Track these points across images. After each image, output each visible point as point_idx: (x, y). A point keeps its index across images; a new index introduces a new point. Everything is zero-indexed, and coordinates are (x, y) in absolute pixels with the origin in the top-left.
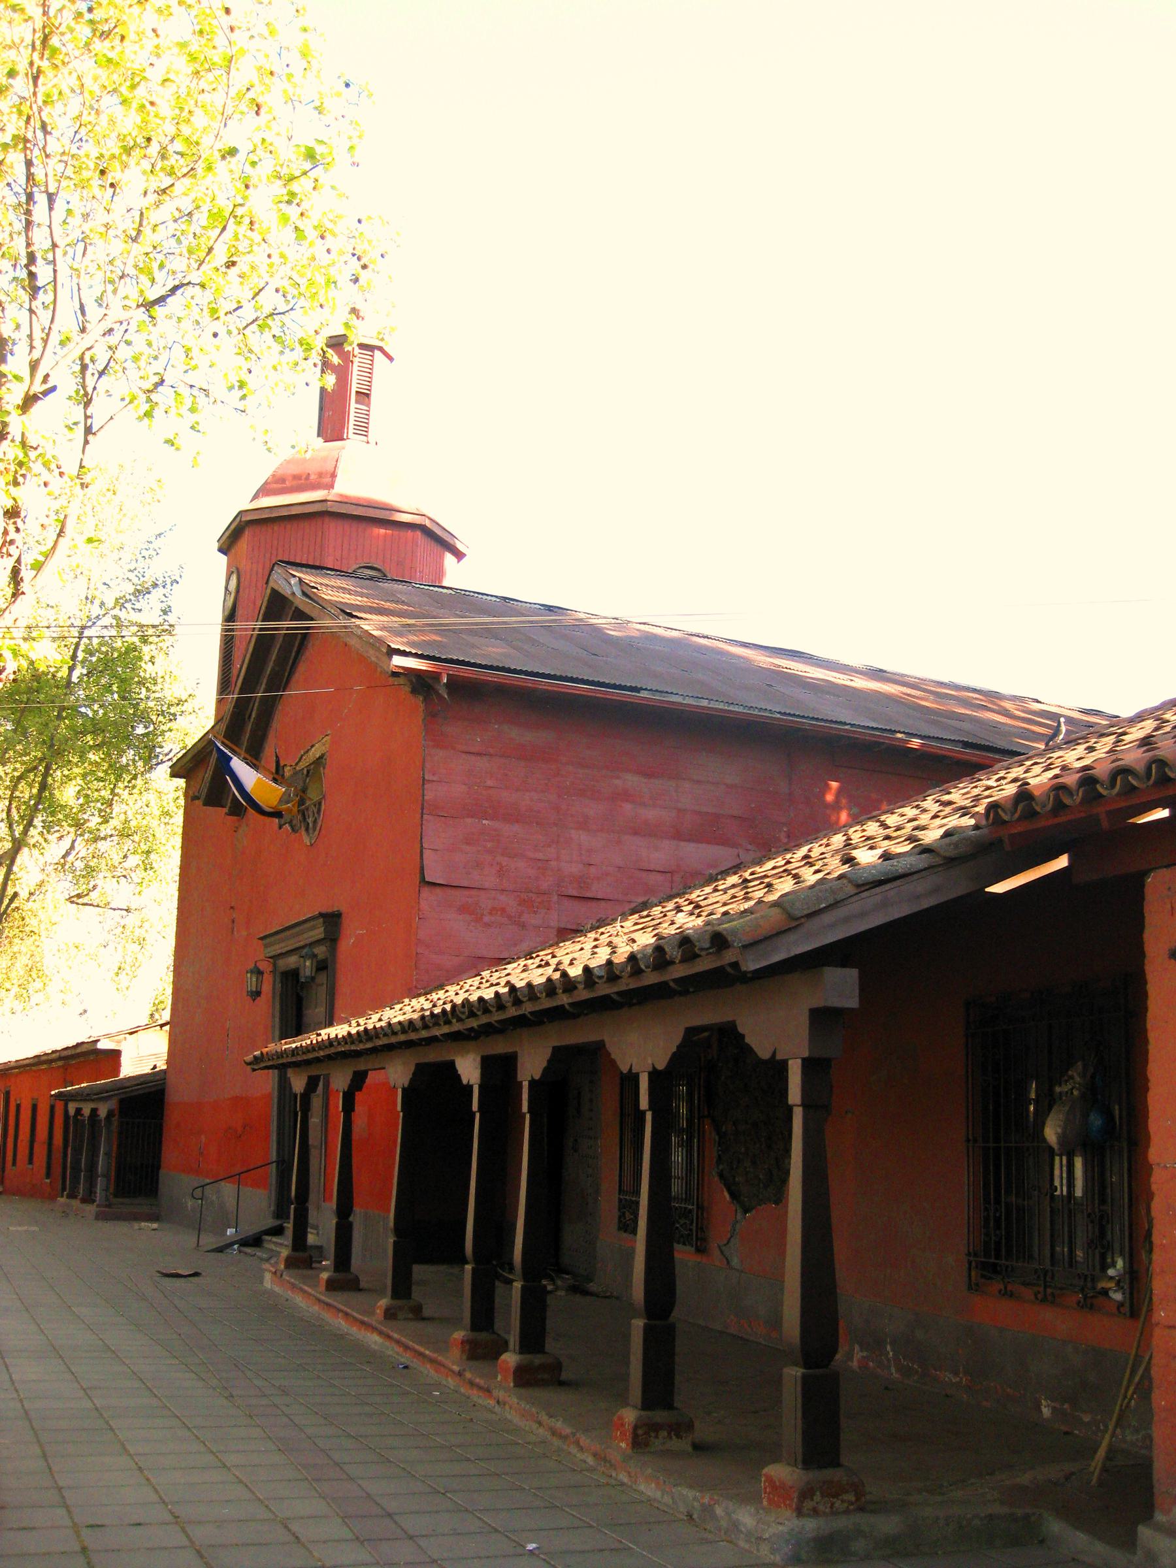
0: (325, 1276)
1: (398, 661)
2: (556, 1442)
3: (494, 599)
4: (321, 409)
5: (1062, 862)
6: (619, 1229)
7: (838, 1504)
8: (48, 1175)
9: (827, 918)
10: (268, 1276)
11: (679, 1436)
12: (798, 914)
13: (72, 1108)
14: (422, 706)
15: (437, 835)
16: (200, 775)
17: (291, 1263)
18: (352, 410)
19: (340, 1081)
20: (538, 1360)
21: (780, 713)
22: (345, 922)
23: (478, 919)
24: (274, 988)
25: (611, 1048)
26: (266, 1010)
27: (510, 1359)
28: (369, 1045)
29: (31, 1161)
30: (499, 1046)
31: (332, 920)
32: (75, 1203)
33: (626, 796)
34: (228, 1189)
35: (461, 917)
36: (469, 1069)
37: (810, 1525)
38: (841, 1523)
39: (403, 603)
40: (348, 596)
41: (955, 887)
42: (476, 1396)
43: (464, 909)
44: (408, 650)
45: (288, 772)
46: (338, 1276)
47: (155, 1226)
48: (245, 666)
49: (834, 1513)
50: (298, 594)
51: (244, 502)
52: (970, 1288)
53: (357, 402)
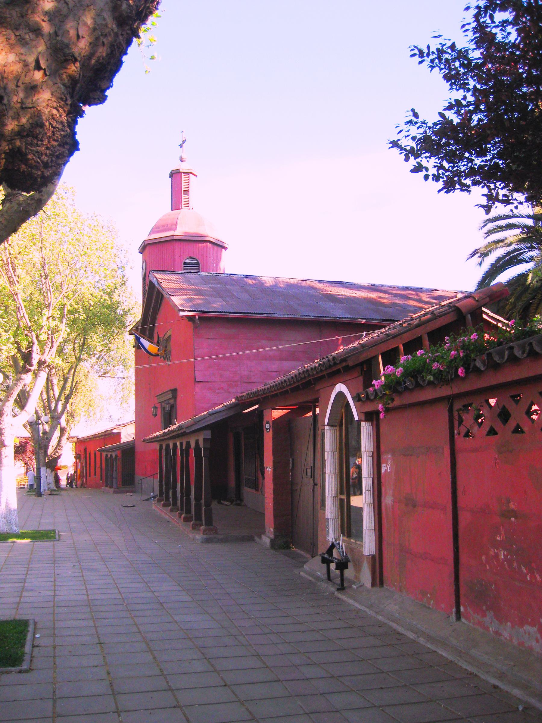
1: (182, 313)
3: (227, 275)
5: (257, 406)
8: (101, 479)
13: (104, 454)
14: (192, 325)
18: (183, 198)
21: (313, 316)
22: (179, 391)
26: (159, 420)
29: (95, 475)
31: (174, 392)
32: (107, 488)
37: (205, 536)
38: (211, 536)
41: (231, 413)
43: (210, 389)
47: (131, 494)
49: (210, 534)
51: (146, 237)
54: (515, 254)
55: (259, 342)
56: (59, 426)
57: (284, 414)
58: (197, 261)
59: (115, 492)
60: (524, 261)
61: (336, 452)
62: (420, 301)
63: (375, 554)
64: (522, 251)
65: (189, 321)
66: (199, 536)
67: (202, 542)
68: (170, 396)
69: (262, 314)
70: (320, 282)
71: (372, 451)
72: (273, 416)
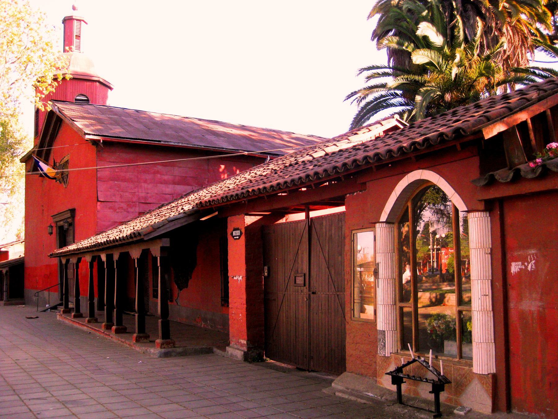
0: (73, 314)
1: (87, 137)
2: (122, 343)
3: (120, 109)
4: (64, 41)
5: (217, 213)
6: (153, 297)
7: (169, 346)
9: (162, 228)
10: (58, 316)
11: (146, 339)
12: (155, 228)
15: (102, 187)
16: (30, 163)
17: (64, 312)
19: (73, 260)
20: (120, 327)
23: (115, 210)
24: (57, 231)
25: (151, 250)
26: (54, 238)
27: (114, 327)
28: (79, 252)
30: (110, 252)
33: (158, 172)
34: (46, 293)
35: (110, 210)
36: (104, 258)
37: (163, 350)
38: (170, 350)
39: (90, 113)
40: (73, 112)
41: (191, 220)
42: (107, 337)
43: (110, 208)
44: (90, 133)
45: (58, 164)
46: (77, 314)
47: (24, 306)
48: (43, 128)
50: (58, 111)
52: (222, 305)
53: (76, 39)
54: (382, 99)
55: (155, 167)
56: (444, 135)
57: (256, 220)
58: (87, 98)
59: (5, 305)
60: (393, 105)
61: (394, 254)
62: (282, 140)
63: (495, 372)
64: (387, 98)
65: (93, 144)
66: (155, 351)
67: (160, 357)
68: (69, 215)
69: (160, 141)
70: (200, 120)
71: (490, 247)
72: (245, 221)
